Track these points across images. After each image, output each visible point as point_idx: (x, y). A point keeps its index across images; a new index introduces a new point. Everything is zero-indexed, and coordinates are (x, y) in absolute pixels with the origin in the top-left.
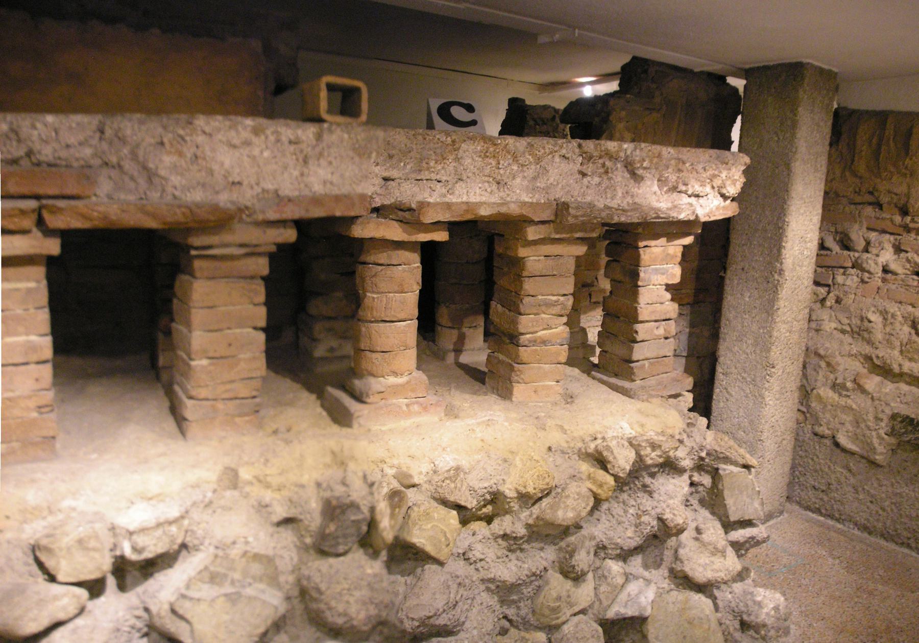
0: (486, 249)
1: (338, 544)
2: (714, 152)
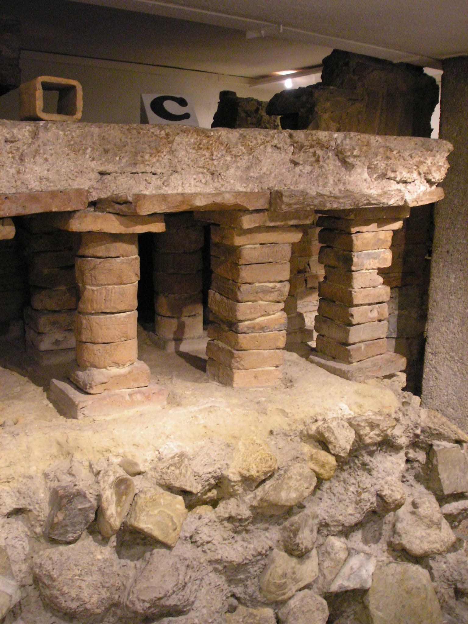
0: (202, 239)
1: (67, 532)
2: (419, 140)
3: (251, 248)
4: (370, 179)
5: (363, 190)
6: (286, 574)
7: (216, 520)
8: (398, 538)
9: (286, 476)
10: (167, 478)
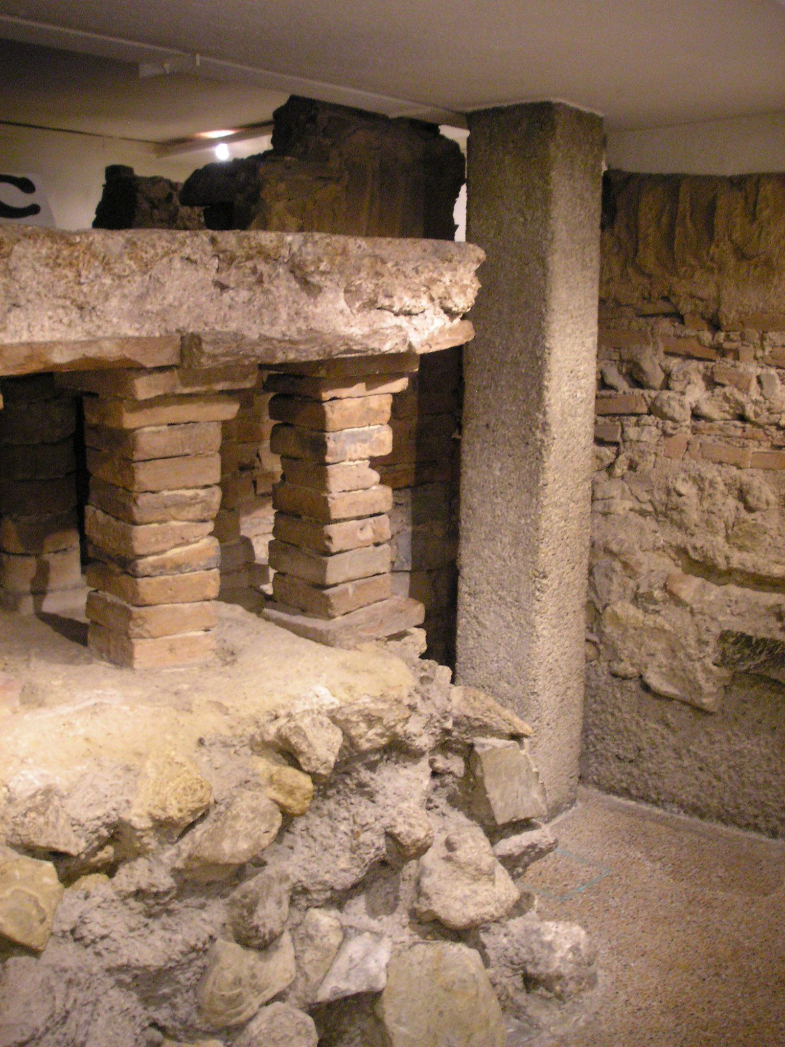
2: (429, 244)
3: (153, 432)
4: (349, 310)
5: (338, 329)
6: (240, 980)
7: (115, 898)
8: (426, 902)
9: (229, 814)
10: (25, 832)
